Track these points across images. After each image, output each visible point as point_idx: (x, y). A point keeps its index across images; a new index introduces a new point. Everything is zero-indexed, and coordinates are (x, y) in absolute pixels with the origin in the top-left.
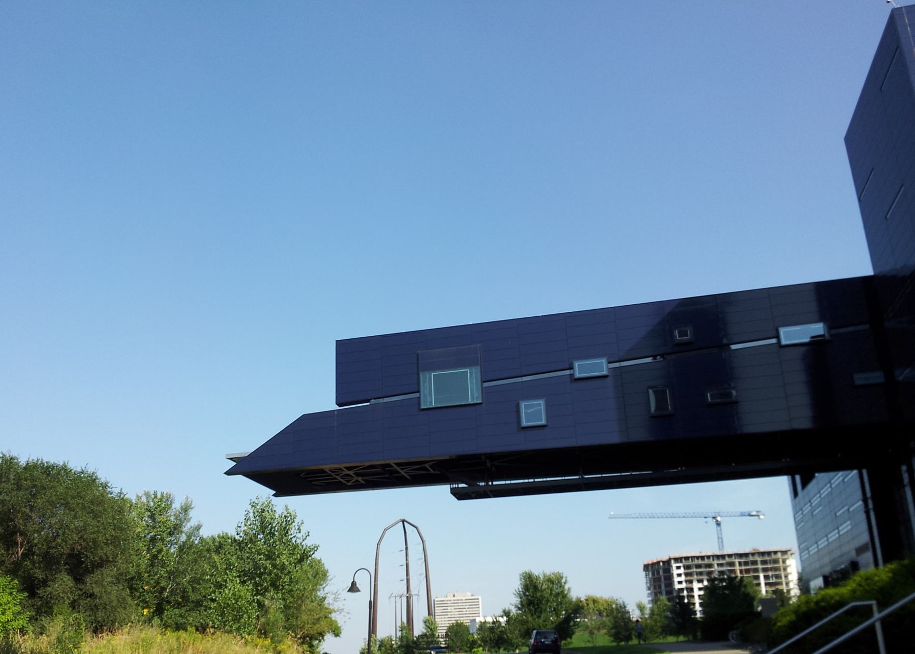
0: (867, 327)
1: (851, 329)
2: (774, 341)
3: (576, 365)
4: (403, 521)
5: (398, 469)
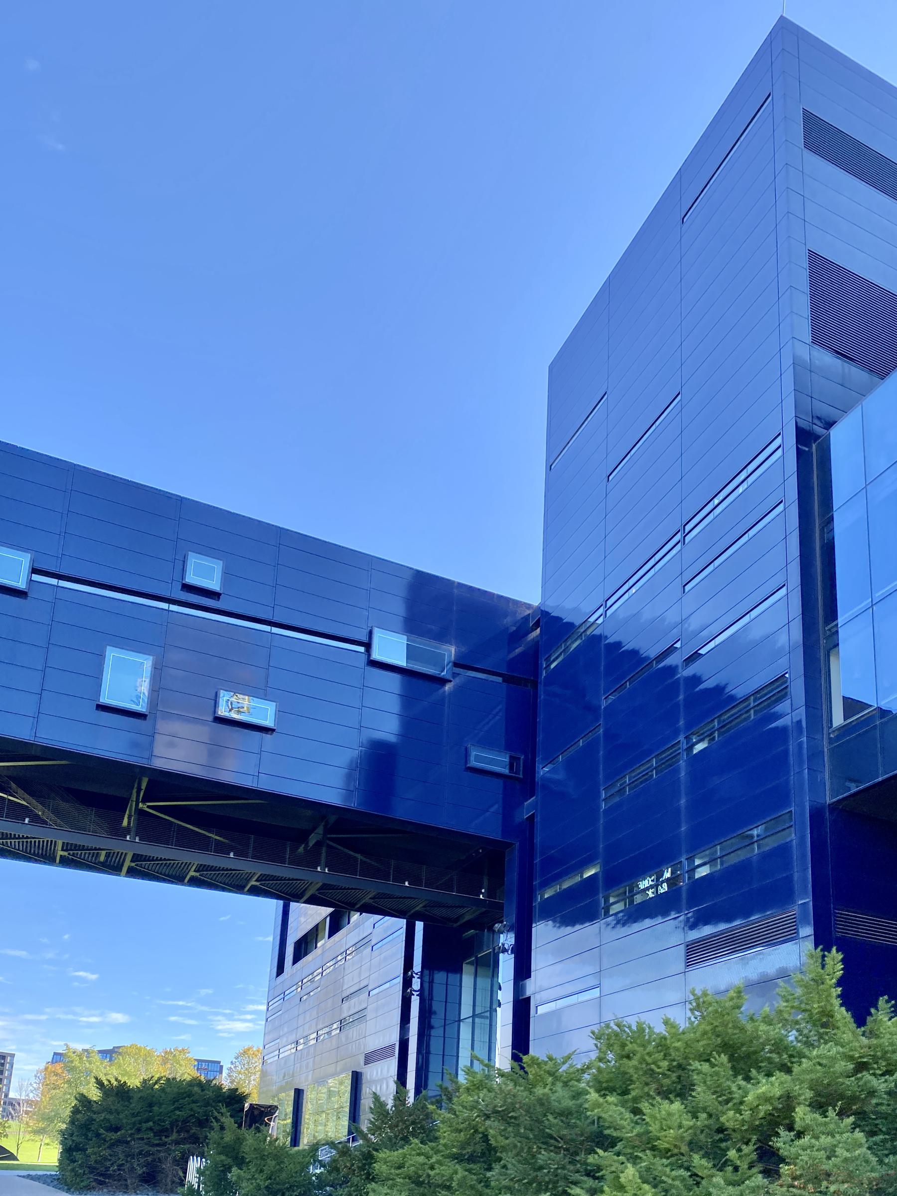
0: (500, 679)
2: (362, 649)
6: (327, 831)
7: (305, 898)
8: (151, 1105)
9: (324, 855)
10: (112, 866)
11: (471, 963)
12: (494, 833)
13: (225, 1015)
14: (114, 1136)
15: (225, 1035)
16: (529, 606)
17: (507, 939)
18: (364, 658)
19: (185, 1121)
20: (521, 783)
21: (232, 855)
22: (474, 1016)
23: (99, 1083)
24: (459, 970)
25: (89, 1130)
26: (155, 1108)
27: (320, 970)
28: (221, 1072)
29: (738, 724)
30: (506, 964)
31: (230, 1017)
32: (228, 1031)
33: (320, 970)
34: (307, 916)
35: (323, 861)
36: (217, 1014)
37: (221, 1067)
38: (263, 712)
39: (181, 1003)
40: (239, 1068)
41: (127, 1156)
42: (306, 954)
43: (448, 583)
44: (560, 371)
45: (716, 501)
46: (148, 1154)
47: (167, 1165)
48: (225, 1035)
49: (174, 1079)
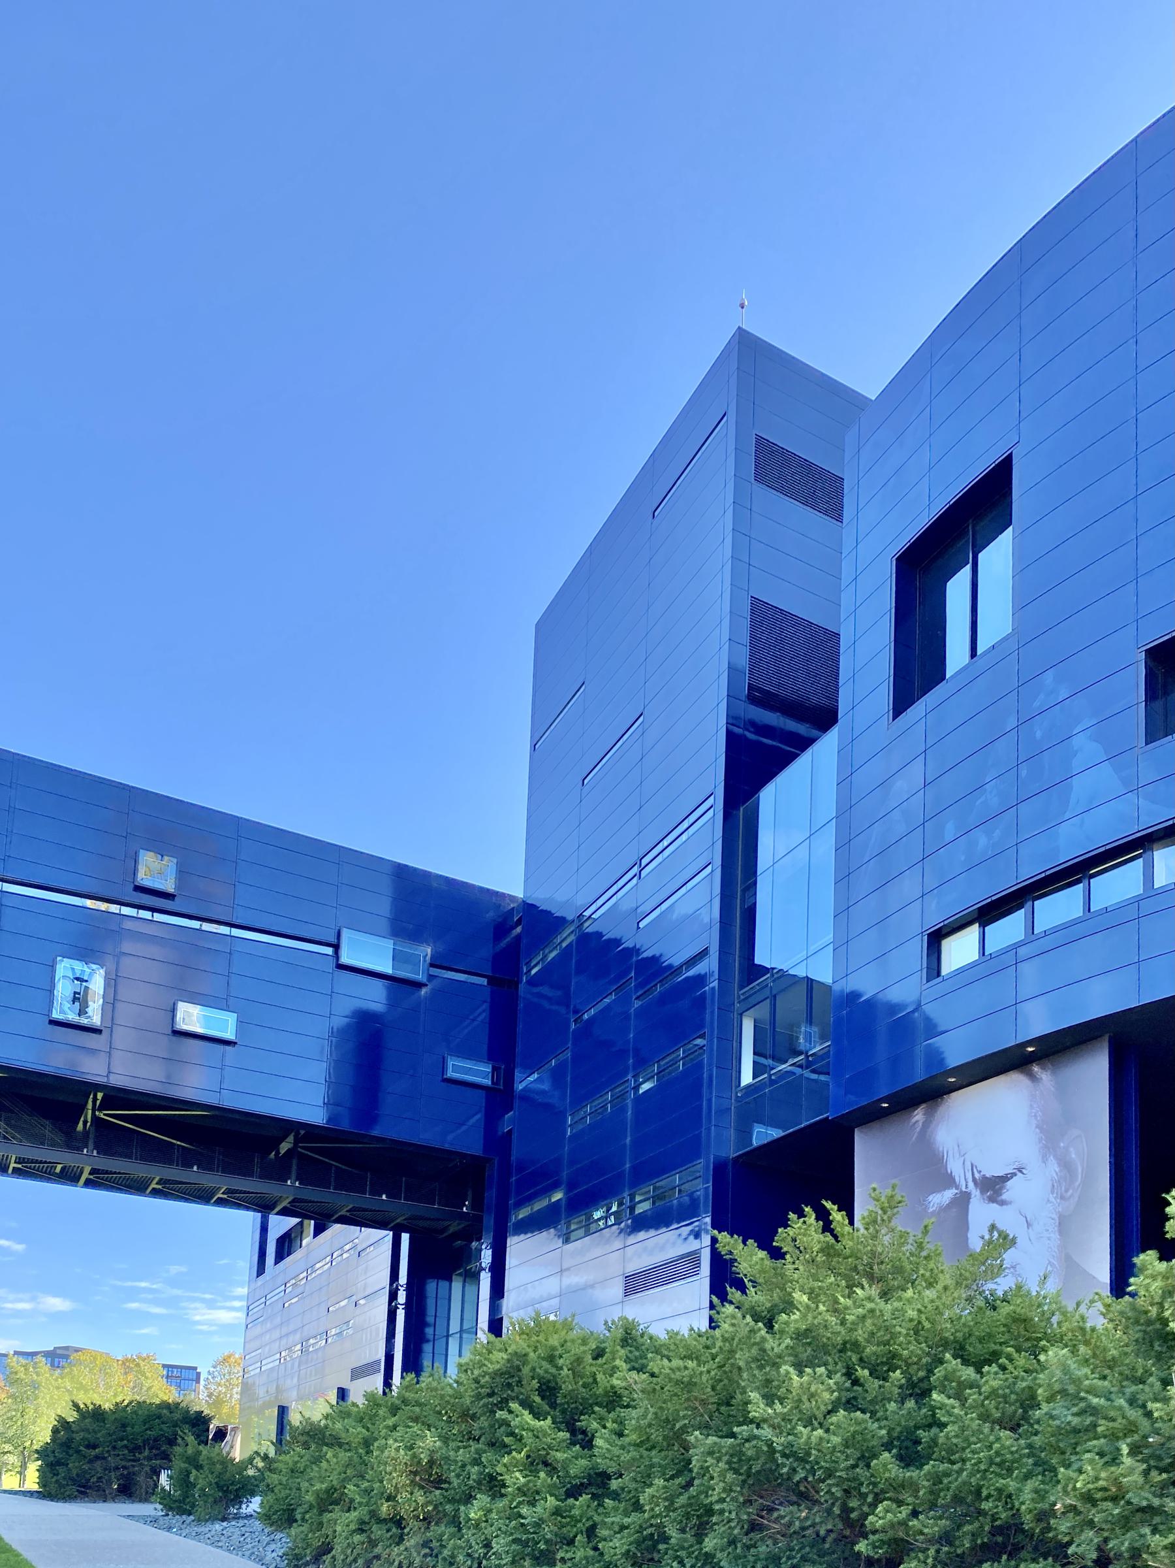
0: (484, 981)
2: (329, 951)
6: (297, 1141)
7: (277, 1210)
8: (124, 1426)
9: (294, 1168)
10: (69, 1176)
11: (460, 1274)
12: (475, 1147)
13: (203, 1301)
14: (93, 1453)
15: (204, 1328)
16: (513, 898)
17: (487, 1257)
19: (156, 1440)
20: (499, 1097)
21: (195, 1168)
22: (461, 1331)
23: (76, 1406)
24: (450, 1280)
25: (69, 1447)
26: (129, 1429)
27: (305, 1274)
28: (198, 1381)
29: (670, 1073)
30: (485, 1279)
31: (211, 1305)
33: (305, 1274)
34: (280, 1224)
35: (294, 1175)
36: (194, 1299)
37: (199, 1374)
38: (225, 1025)
39: (143, 1284)
40: (218, 1379)
41: (105, 1469)
42: (289, 1254)
43: (426, 875)
44: (549, 630)
45: (665, 843)
46: (124, 1468)
47: (141, 1479)
48: (204, 1328)
49: (144, 1402)
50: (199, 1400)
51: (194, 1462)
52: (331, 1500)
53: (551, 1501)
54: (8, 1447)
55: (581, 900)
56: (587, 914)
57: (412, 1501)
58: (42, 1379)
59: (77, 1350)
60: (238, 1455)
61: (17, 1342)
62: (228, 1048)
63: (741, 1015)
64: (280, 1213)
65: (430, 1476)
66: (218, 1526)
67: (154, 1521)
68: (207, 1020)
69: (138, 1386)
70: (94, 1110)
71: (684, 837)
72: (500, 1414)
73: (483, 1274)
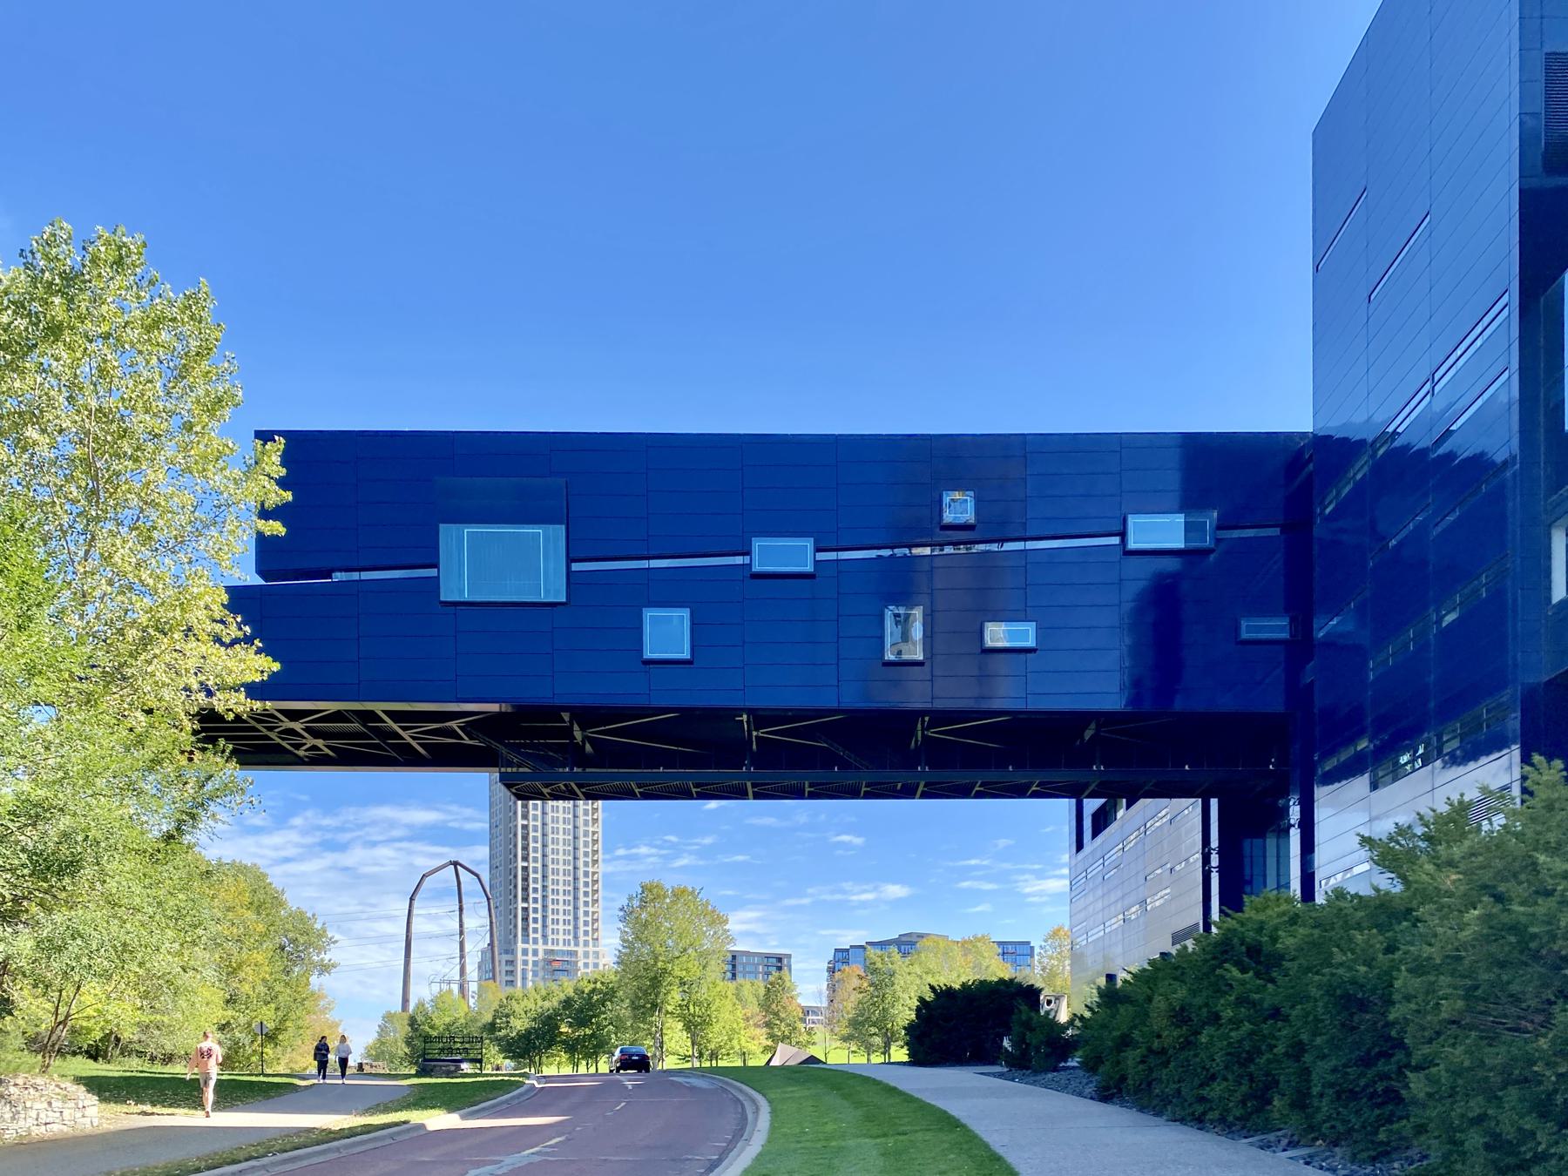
0: (1275, 532)
1: (1250, 533)
2: (1116, 540)
3: (757, 544)
4: (456, 864)
5: (395, 727)
12: (1275, 703)
17: (1295, 813)
18: (1119, 551)
20: (1300, 647)
23: (932, 987)
28: (1032, 955)
30: (1295, 835)
31: (1041, 875)
32: (1041, 894)
34: (1092, 805)
36: (1023, 872)
37: (1032, 948)
39: (973, 862)
44: (1326, 137)
45: (1459, 352)
50: (1032, 975)
51: (1028, 1026)
52: (1125, 1042)
53: (1247, 1026)
54: (873, 1030)
55: (1379, 418)
56: (1390, 430)
57: (1171, 1035)
58: (895, 967)
59: (921, 936)
60: (1063, 1017)
61: (863, 933)
62: (1029, 655)
63: (1550, 526)
64: (1088, 797)
65: (1180, 1016)
66: (1050, 1076)
67: (1000, 1075)
68: (1011, 635)
69: (977, 966)
70: (923, 730)
71: (1479, 343)
72: (1218, 971)
73: (1293, 831)
